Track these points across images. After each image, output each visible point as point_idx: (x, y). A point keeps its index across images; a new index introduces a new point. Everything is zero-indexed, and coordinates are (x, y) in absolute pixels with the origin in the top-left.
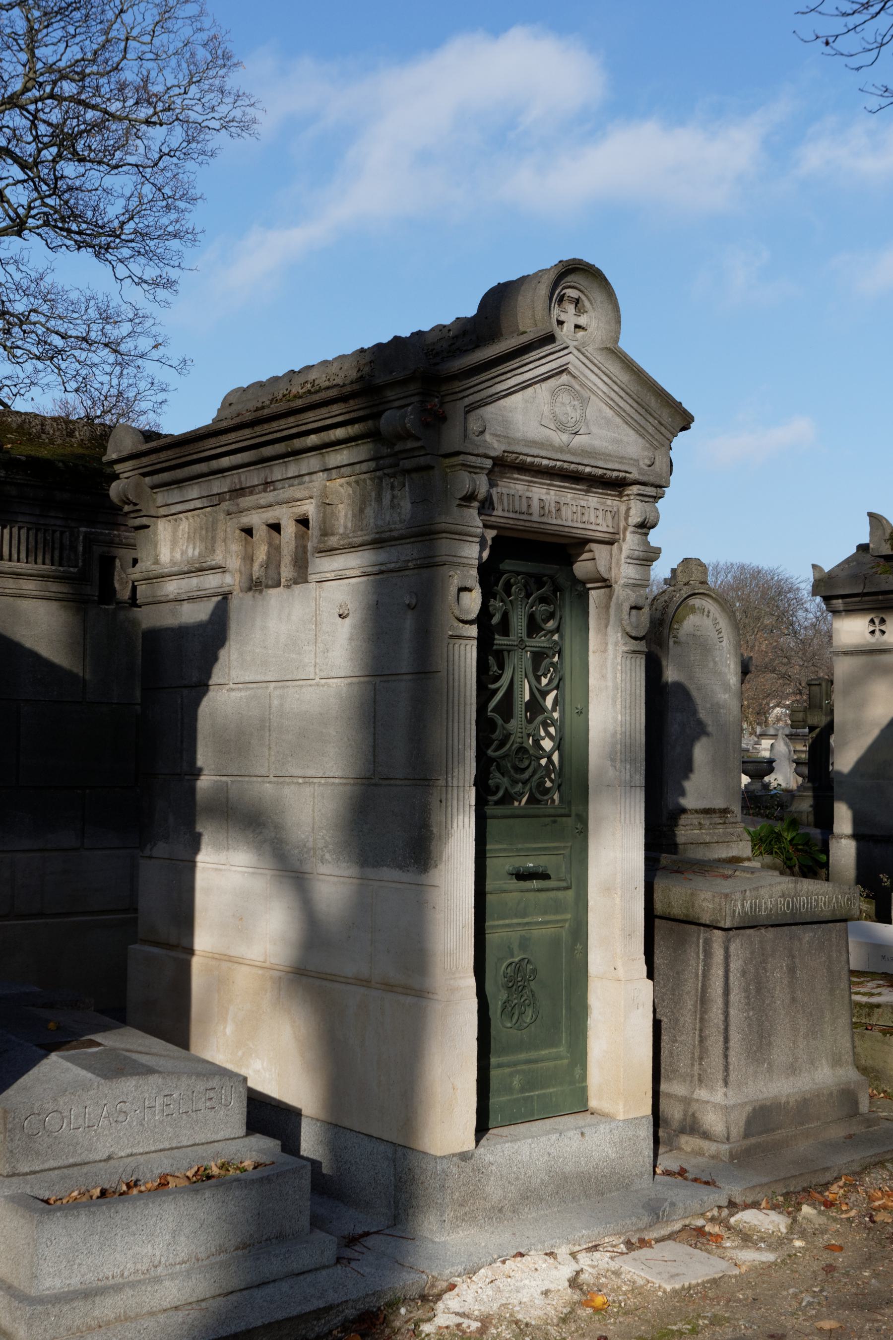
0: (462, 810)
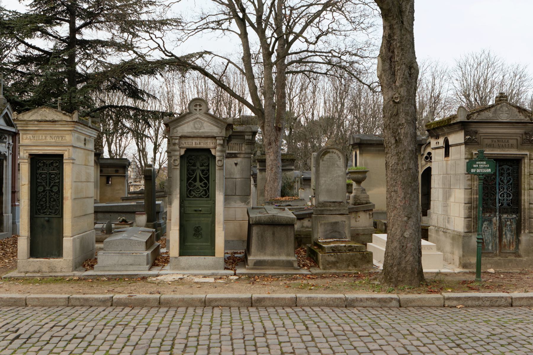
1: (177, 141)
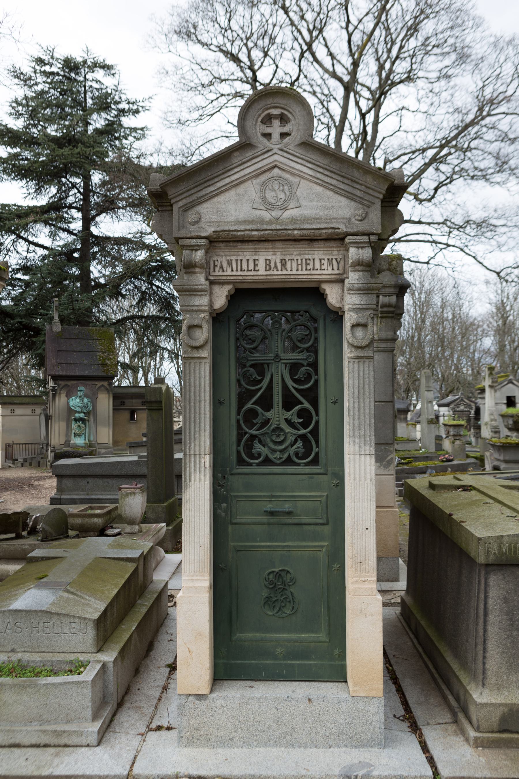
0: (198, 471)
1: (199, 255)
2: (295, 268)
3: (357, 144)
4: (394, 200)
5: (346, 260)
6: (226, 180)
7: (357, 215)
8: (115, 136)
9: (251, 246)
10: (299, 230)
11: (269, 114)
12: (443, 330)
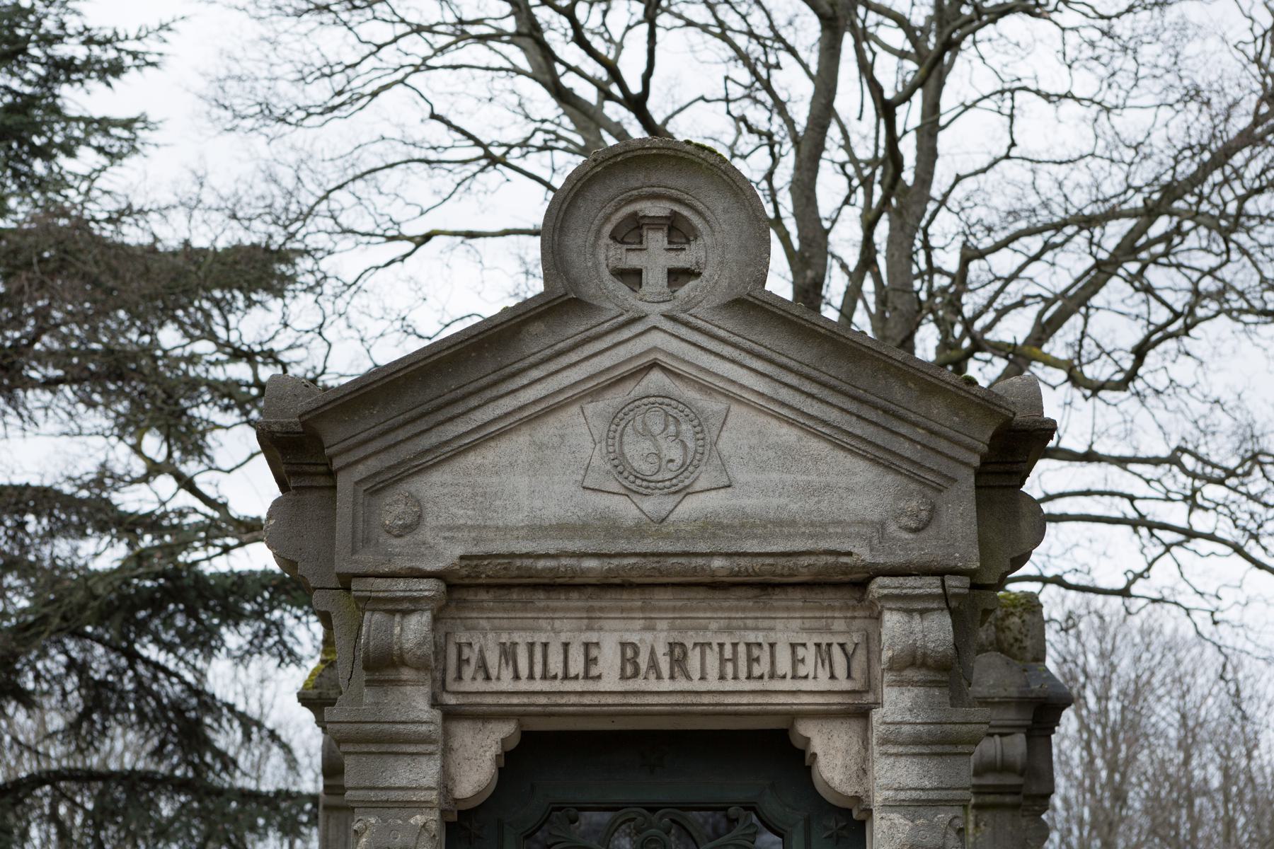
1: (414, 630)
2: (713, 671)
3: (869, 195)
4: (1015, 468)
5: (874, 648)
6: (502, 402)
7: (903, 512)
8: (32, 145)
9: (576, 600)
10: (728, 555)
11: (635, 213)
12: (1193, 830)
